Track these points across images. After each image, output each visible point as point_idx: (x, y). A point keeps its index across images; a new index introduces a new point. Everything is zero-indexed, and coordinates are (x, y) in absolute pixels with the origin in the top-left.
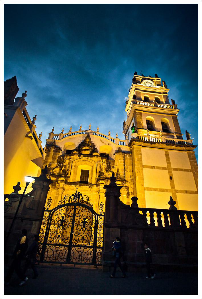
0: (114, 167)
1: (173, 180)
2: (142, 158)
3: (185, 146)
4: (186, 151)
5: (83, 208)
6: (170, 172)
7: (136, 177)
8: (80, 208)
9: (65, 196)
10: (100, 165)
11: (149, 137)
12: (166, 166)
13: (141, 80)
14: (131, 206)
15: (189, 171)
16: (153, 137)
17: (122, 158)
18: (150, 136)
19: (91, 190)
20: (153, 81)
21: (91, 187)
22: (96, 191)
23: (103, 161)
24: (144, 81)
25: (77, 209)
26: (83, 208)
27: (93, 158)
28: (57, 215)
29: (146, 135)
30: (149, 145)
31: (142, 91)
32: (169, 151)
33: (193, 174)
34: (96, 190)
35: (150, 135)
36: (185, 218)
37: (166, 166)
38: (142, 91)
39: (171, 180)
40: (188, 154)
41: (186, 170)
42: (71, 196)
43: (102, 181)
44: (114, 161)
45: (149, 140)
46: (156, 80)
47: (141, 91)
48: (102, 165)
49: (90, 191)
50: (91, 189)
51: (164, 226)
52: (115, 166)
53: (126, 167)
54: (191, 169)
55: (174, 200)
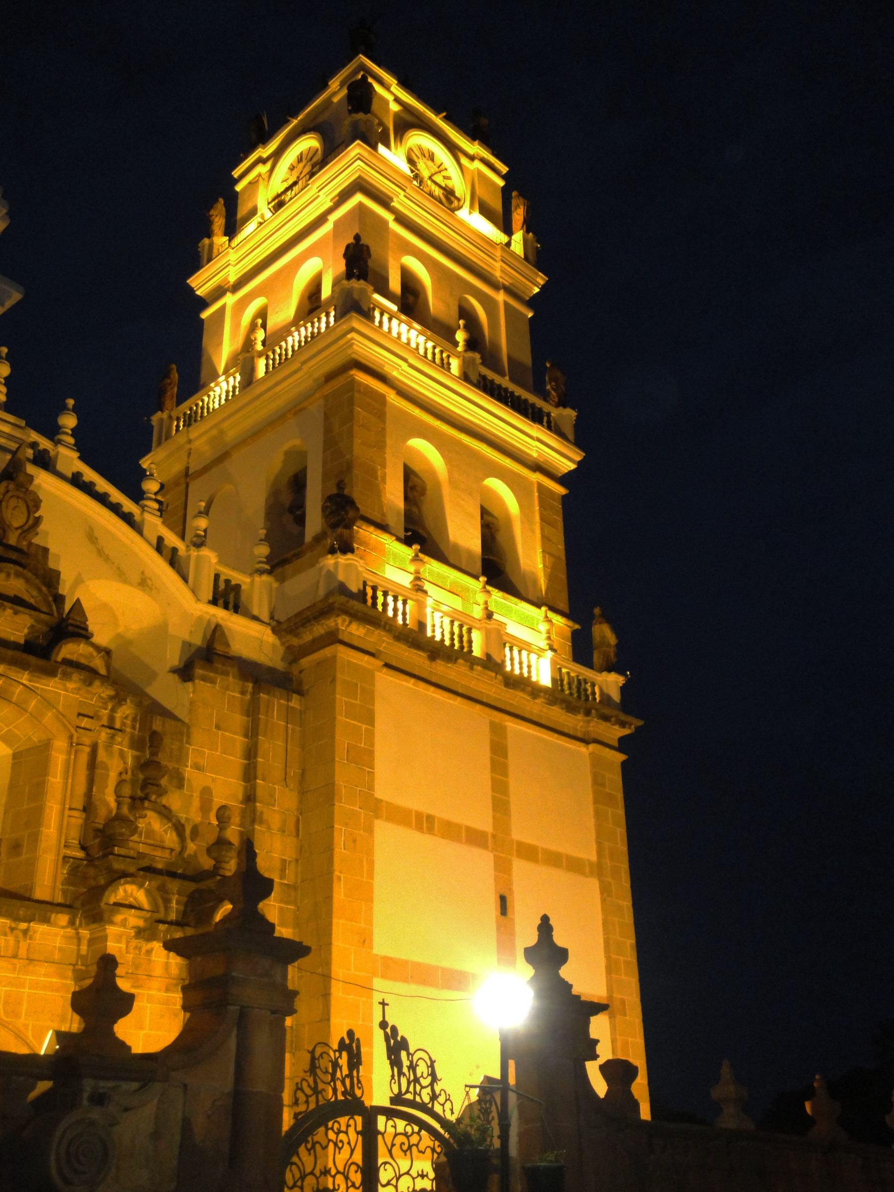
0: (180, 781)
1: (512, 920)
2: (372, 745)
3: (588, 713)
4: (585, 741)
5: (409, 1129)
6: (502, 868)
7: (335, 880)
8: (395, 1127)
9: (312, 1052)
10: (94, 749)
11: (421, 606)
12: (483, 822)
13: (397, 115)
14: (645, 1113)
15: (587, 870)
16: (444, 608)
17: (238, 720)
18: (429, 602)
19: (22, 952)
20: (464, 161)
21: (23, 925)
22: (57, 956)
23: (112, 719)
24: (418, 139)
25: (383, 1134)
26: (409, 1129)
27: (52, 686)
28: (394, 1182)
29: (405, 580)
30: (417, 659)
31: (402, 220)
32: (513, 726)
33: (602, 893)
34: (61, 950)
35: (427, 586)
36: (499, 1137)
37: (483, 822)
38: (402, 220)
39: (503, 917)
40: (594, 757)
41: (574, 865)
42: (337, 1054)
43: (131, 888)
44: (183, 730)
45: (422, 625)
46: (477, 164)
47: (389, 217)
48: (109, 746)
49: (15, 956)
50: (24, 945)
51: (645, 1113)
52: (188, 772)
53: (260, 793)
54: (594, 858)
55: (124, 985)
